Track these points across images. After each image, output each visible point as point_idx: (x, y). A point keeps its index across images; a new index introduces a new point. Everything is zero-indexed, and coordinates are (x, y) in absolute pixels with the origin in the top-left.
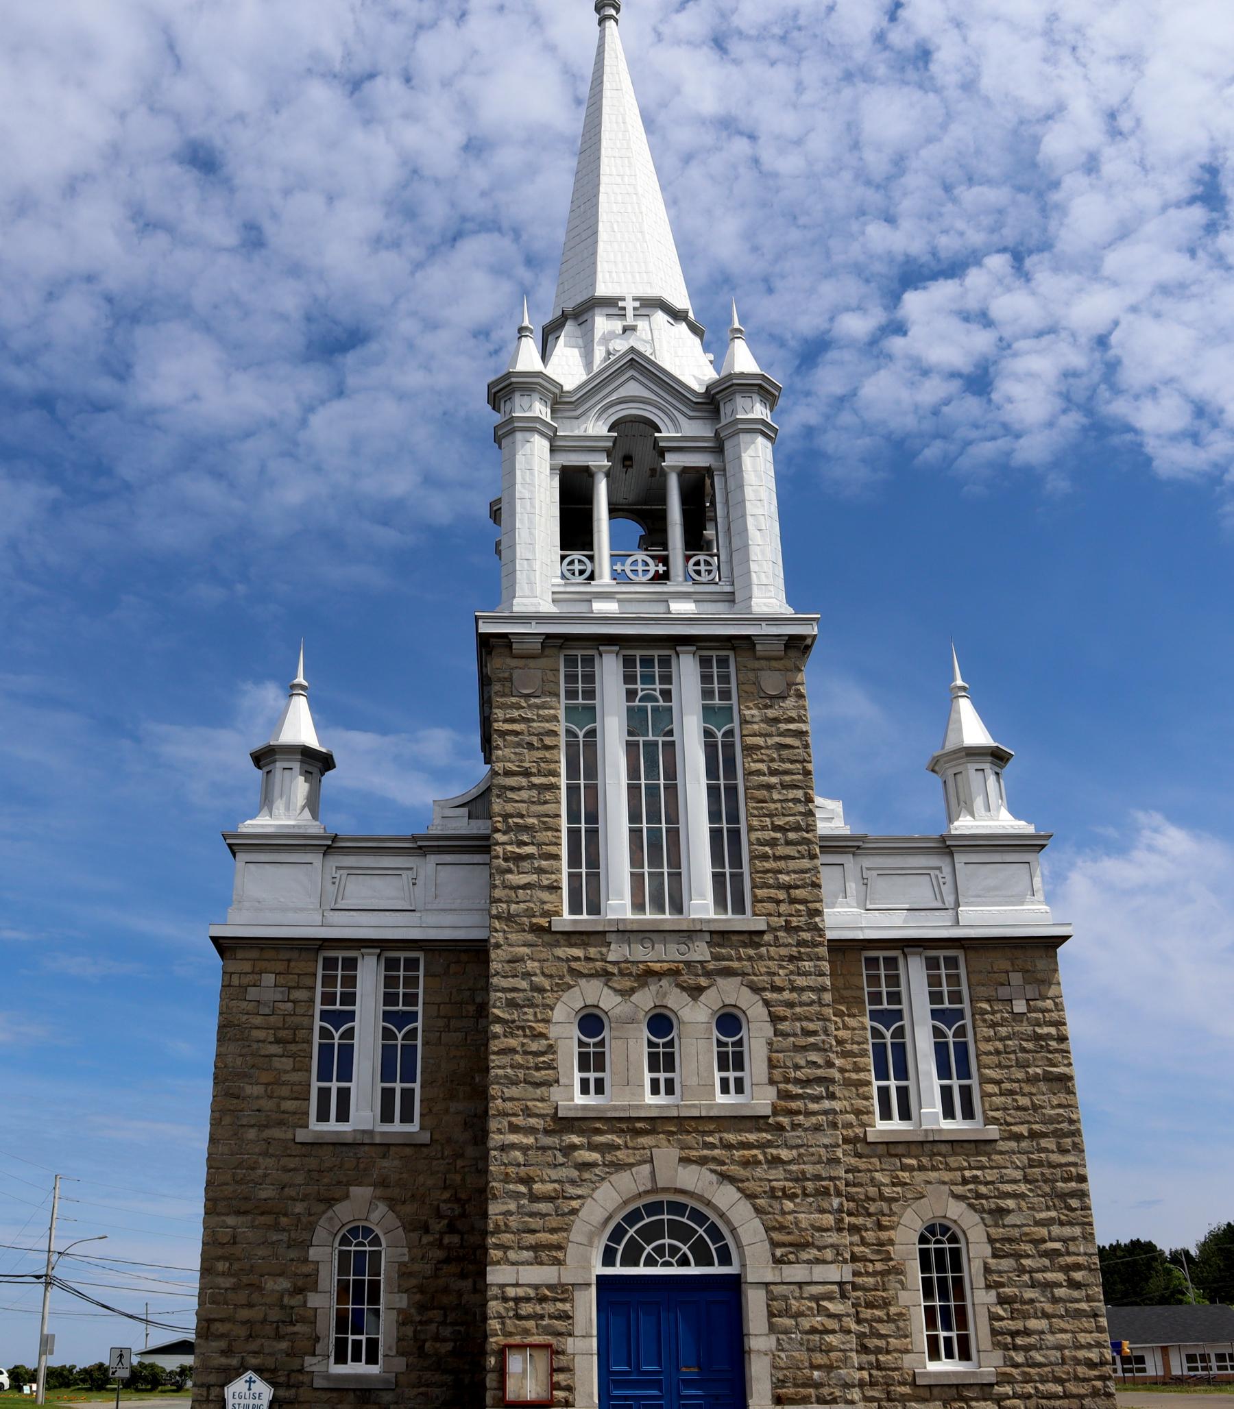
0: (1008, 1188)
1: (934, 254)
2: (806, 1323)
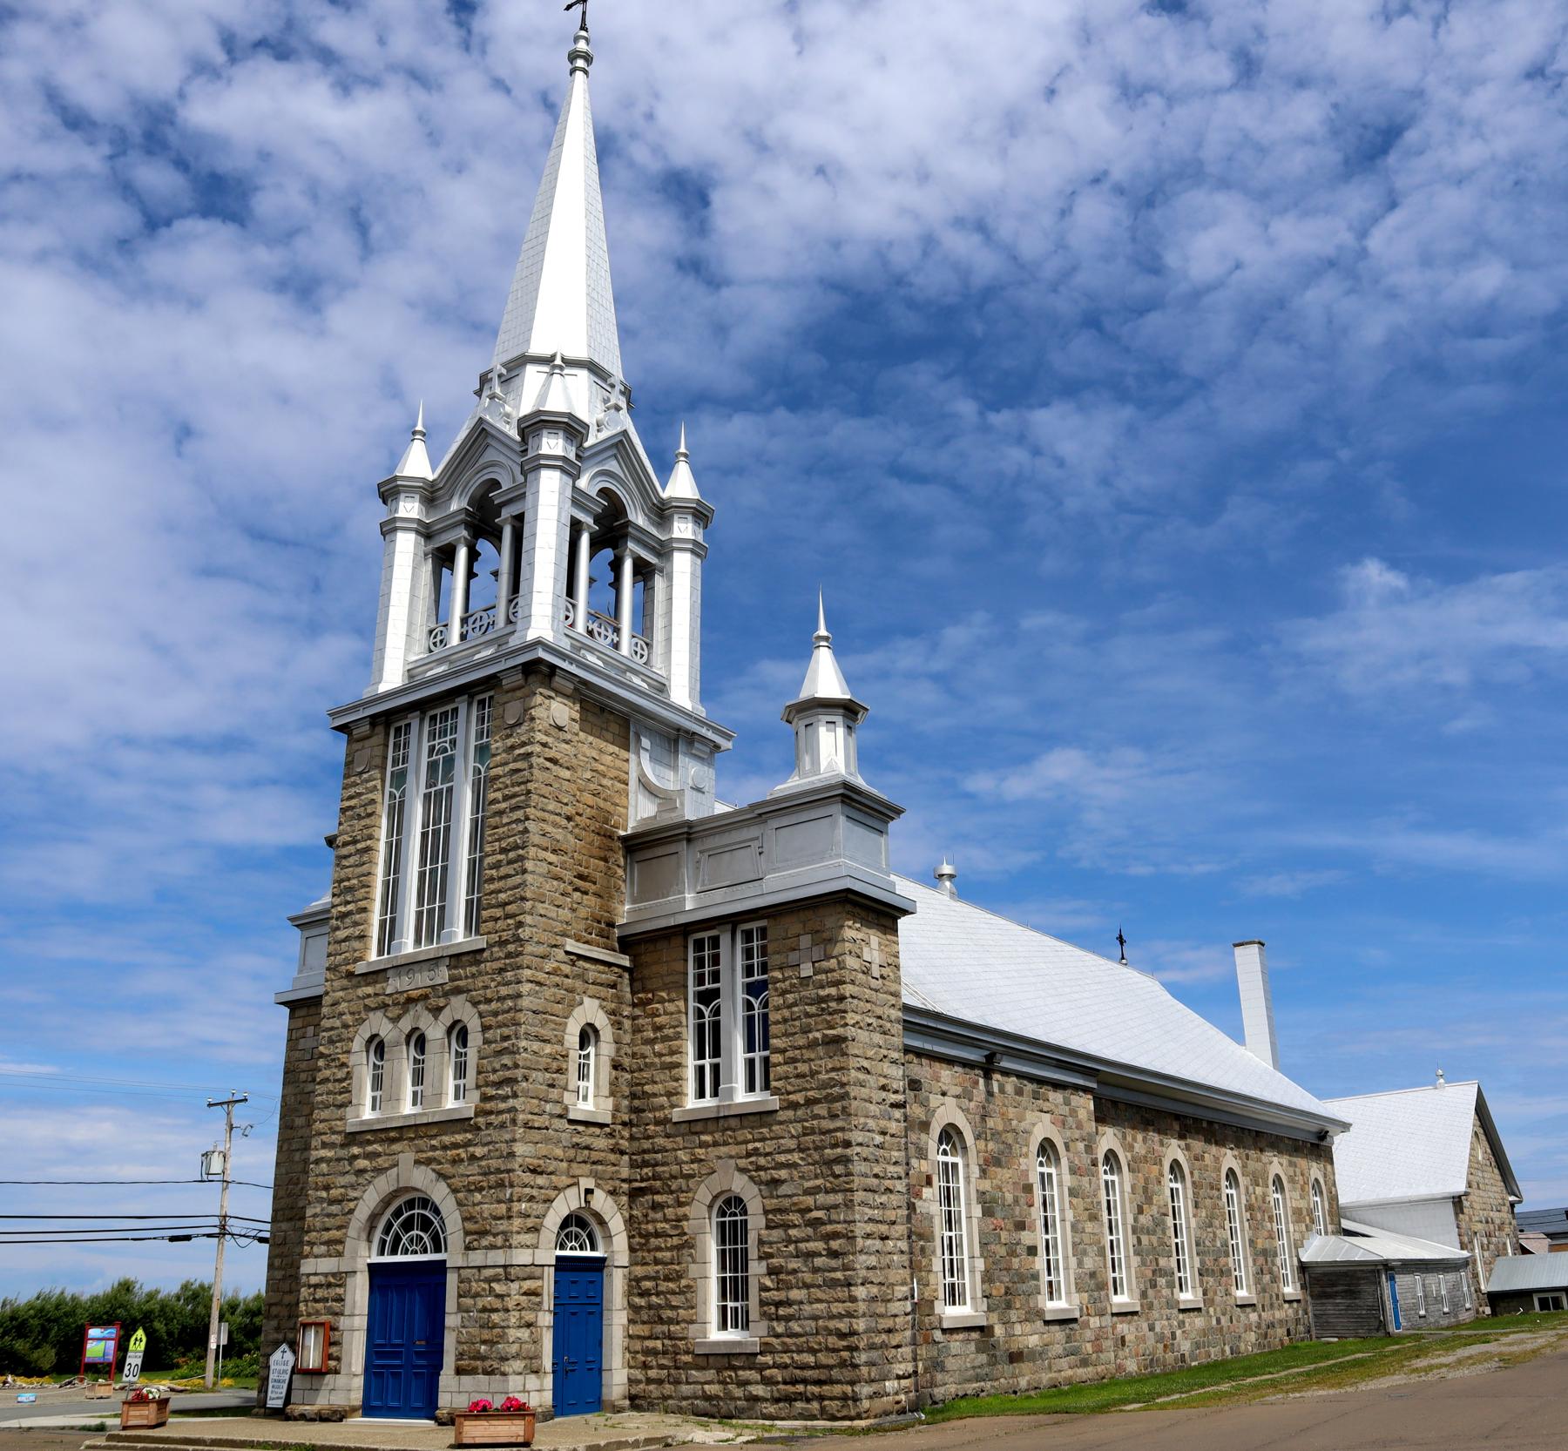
0: (782, 1158)
2: (480, 1303)
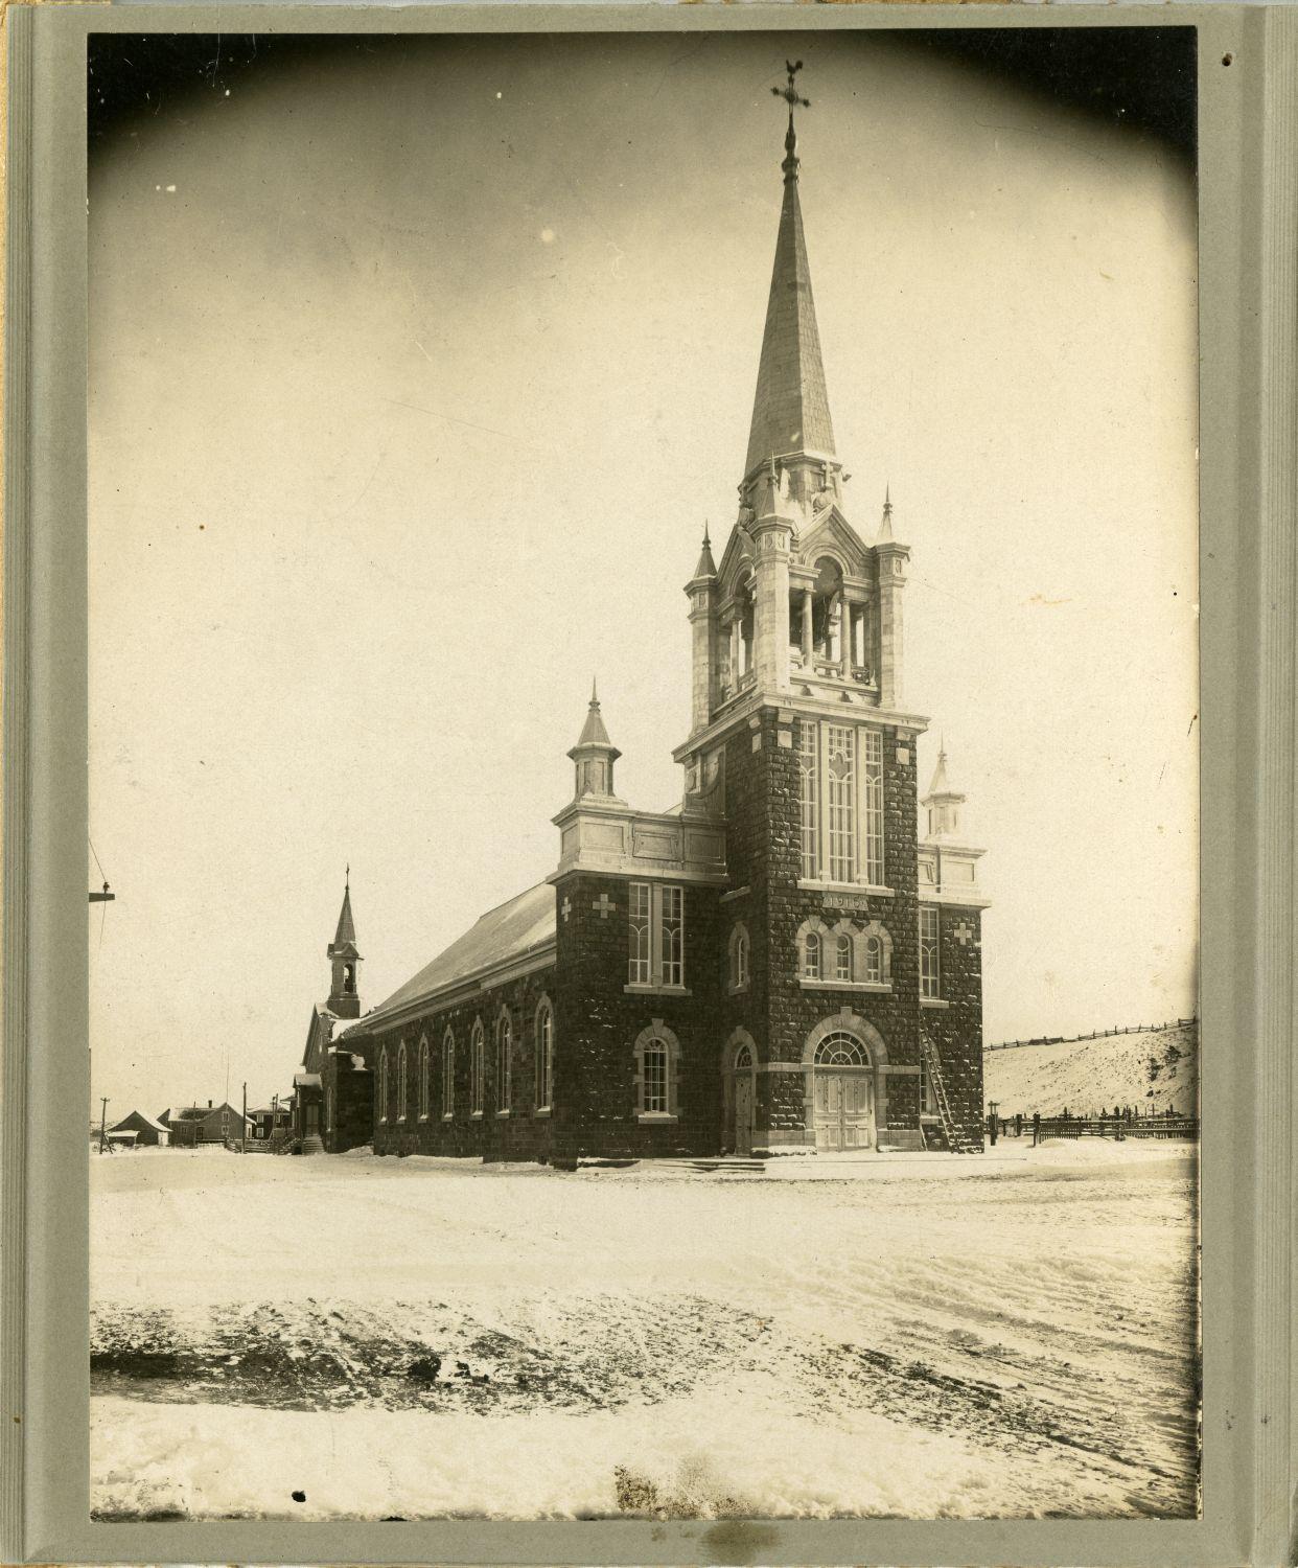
1: (1186, 1334)
